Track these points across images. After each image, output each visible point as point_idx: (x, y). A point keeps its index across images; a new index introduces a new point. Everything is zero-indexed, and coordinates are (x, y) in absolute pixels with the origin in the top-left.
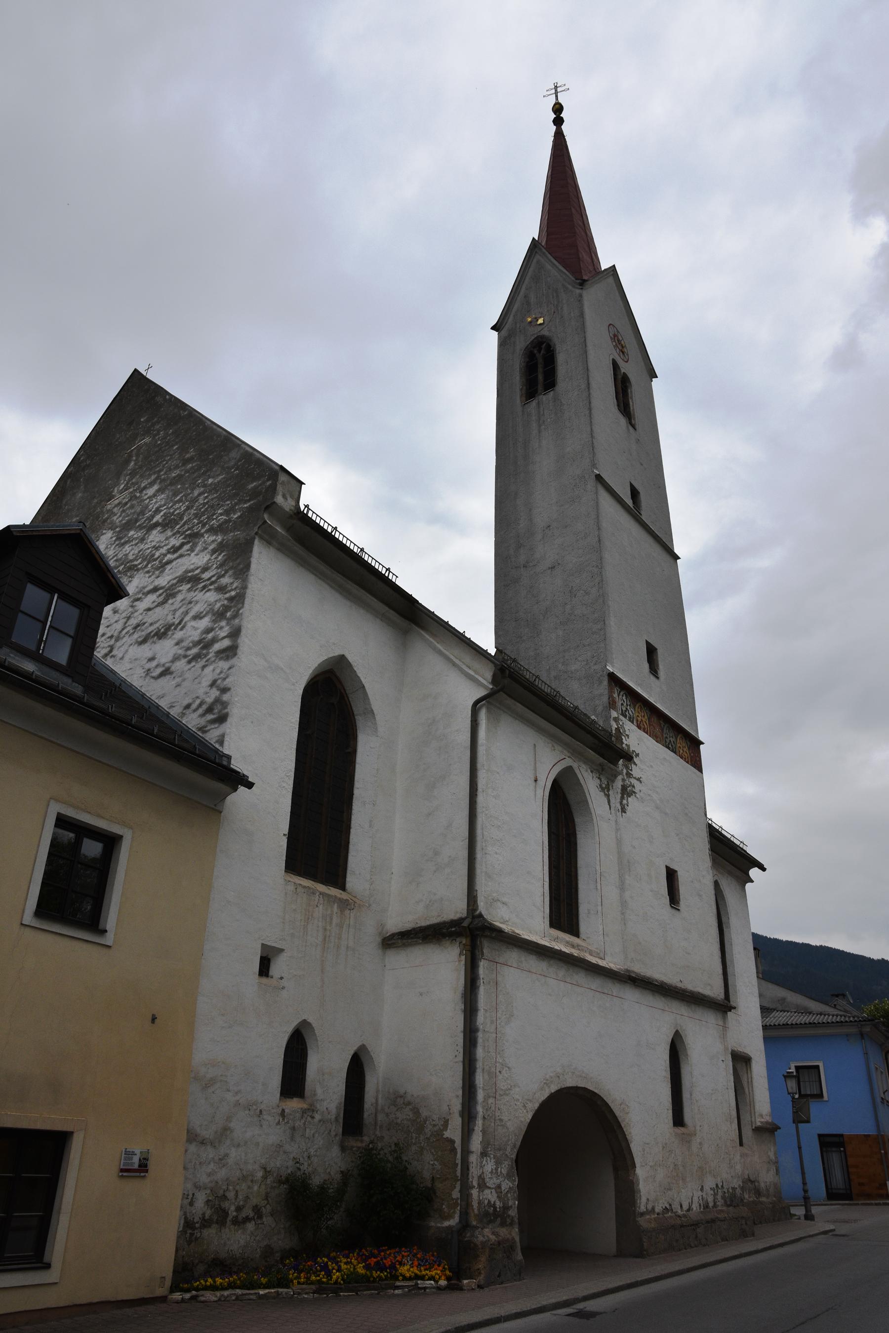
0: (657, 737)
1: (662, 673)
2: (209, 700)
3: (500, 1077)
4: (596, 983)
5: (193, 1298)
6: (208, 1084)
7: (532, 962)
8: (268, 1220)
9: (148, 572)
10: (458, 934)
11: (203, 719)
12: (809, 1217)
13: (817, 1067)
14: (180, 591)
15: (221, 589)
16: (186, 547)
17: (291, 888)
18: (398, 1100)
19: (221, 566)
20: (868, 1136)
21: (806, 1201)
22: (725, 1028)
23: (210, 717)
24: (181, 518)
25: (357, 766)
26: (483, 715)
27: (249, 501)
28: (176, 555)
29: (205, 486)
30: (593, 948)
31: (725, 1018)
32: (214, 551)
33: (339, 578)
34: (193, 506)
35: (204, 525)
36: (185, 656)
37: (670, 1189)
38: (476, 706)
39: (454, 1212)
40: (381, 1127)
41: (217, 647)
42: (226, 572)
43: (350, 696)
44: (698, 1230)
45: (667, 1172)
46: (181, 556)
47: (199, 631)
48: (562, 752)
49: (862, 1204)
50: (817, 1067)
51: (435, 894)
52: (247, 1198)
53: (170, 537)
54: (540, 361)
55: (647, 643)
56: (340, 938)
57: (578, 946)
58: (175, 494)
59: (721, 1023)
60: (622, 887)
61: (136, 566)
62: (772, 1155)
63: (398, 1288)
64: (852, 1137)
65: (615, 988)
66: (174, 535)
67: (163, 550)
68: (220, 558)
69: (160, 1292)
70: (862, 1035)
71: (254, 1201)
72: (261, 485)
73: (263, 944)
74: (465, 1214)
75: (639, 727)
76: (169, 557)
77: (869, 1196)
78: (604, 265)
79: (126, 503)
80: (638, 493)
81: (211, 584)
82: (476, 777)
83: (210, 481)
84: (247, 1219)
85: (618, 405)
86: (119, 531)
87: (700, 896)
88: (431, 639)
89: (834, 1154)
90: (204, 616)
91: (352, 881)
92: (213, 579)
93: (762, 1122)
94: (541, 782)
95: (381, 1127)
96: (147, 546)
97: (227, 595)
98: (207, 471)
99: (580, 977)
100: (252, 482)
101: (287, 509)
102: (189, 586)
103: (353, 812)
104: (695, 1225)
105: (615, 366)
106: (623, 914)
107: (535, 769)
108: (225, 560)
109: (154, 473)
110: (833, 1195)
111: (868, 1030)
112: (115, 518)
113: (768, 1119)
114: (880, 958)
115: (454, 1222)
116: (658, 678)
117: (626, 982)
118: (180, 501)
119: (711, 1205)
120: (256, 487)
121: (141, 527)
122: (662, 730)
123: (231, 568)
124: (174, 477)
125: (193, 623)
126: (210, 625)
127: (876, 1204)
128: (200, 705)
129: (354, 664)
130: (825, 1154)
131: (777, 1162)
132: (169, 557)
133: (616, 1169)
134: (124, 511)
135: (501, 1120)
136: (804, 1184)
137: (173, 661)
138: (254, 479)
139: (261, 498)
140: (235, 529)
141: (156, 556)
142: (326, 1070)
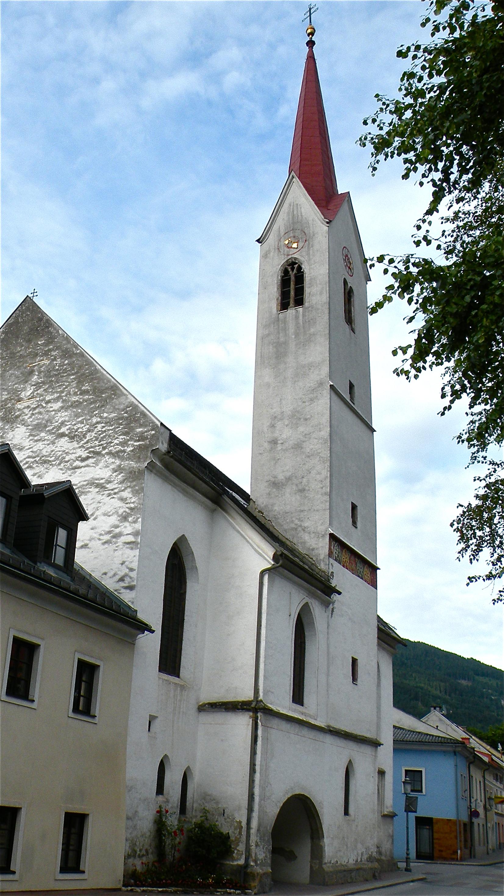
0: (353, 570)
1: (359, 524)
2: (121, 574)
3: (267, 789)
4: (312, 734)
5: (132, 890)
6: (130, 789)
7: (284, 725)
8: (150, 856)
9: (61, 469)
10: (248, 710)
11: (118, 584)
12: (408, 870)
13: (421, 771)
14: (89, 492)
15: (122, 499)
16: (91, 461)
17: (161, 681)
18: (205, 797)
19: (121, 482)
20: (450, 820)
21: (407, 860)
22: (376, 756)
23: (122, 584)
24: (84, 436)
25: (186, 602)
26: (266, 578)
27: (139, 441)
28: (83, 464)
29: (101, 417)
30: (311, 713)
31: (376, 751)
32: (115, 471)
33: (184, 486)
34: (93, 431)
35: (104, 448)
36: (99, 539)
37: (340, 851)
38: (262, 574)
39: (241, 858)
40: (196, 811)
41: (123, 539)
42: (126, 488)
43: (184, 558)
44: (352, 874)
45: (344, 841)
46: (88, 466)
47: (109, 525)
48: (303, 594)
49: (440, 863)
50: (421, 771)
51: (232, 684)
52: (143, 845)
53: (77, 448)
54: (293, 278)
55: (352, 502)
56: (180, 708)
57: (305, 713)
58: (77, 415)
59: (373, 754)
60: (328, 675)
61: (50, 461)
62: (390, 831)
63: (218, 892)
64: (438, 820)
65: (321, 736)
66: (80, 447)
67: (73, 457)
68: (119, 477)
69: (120, 886)
70: (455, 753)
71: (146, 847)
72: (146, 432)
73: (150, 715)
74: (247, 859)
75: (344, 566)
76: (78, 463)
77: (445, 859)
78: (341, 190)
79: (34, 409)
80: (354, 386)
81: (115, 494)
82: (261, 618)
83: (105, 415)
84: (143, 855)
85: (345, 318)
86: (32, 430)
87: (369, 674)
88: (229, 519)
89: (425, 830)
90: (112, 515)
91: (183, 672)
92: (116, 491)
93: (387, 812)
94: (292, 616)
95: (196, 811)
96: (57, 449)
97: (128, 505)
98: (103, 406)
99: (305, 731)
100: (140, 428)
101: (163, 451)
102: (97, 490)
103: (184, 630)
104: (351, 871)
105: (345, 282)
106: (327, 691)
107: (290, 609)
108: (124, 480)
109: (57, 392)
110: (420, 856)
111: (460, 749)
112: (26, 417)
113: (391, 810)
114: (469, 657)
115: (242, 862)
116: (356, 528)
117: (326, 733)
118: (82, 422)
119: (359, 860)
120: (143, 433)
121: (50, 432)
122: (356, 564)
123: (129, 487)
124: (75, 402)
125: (103, 518)
126: (117, 523)
127: (449, 864)
128: (115, 575)
129: (188, 539)
130: (418, 830)
131: (393, 836)
132: (78, 463)
133: (312, 838)
134: (33, 414)
135: (266, 812)
136: (408, 849)
137: (90, 540)
138: (141, 426)
139: (147, 442)
140: (129, 459)
141: (66, 459)
142: (173, 779)
